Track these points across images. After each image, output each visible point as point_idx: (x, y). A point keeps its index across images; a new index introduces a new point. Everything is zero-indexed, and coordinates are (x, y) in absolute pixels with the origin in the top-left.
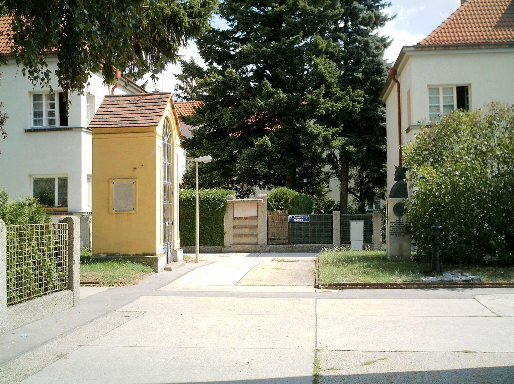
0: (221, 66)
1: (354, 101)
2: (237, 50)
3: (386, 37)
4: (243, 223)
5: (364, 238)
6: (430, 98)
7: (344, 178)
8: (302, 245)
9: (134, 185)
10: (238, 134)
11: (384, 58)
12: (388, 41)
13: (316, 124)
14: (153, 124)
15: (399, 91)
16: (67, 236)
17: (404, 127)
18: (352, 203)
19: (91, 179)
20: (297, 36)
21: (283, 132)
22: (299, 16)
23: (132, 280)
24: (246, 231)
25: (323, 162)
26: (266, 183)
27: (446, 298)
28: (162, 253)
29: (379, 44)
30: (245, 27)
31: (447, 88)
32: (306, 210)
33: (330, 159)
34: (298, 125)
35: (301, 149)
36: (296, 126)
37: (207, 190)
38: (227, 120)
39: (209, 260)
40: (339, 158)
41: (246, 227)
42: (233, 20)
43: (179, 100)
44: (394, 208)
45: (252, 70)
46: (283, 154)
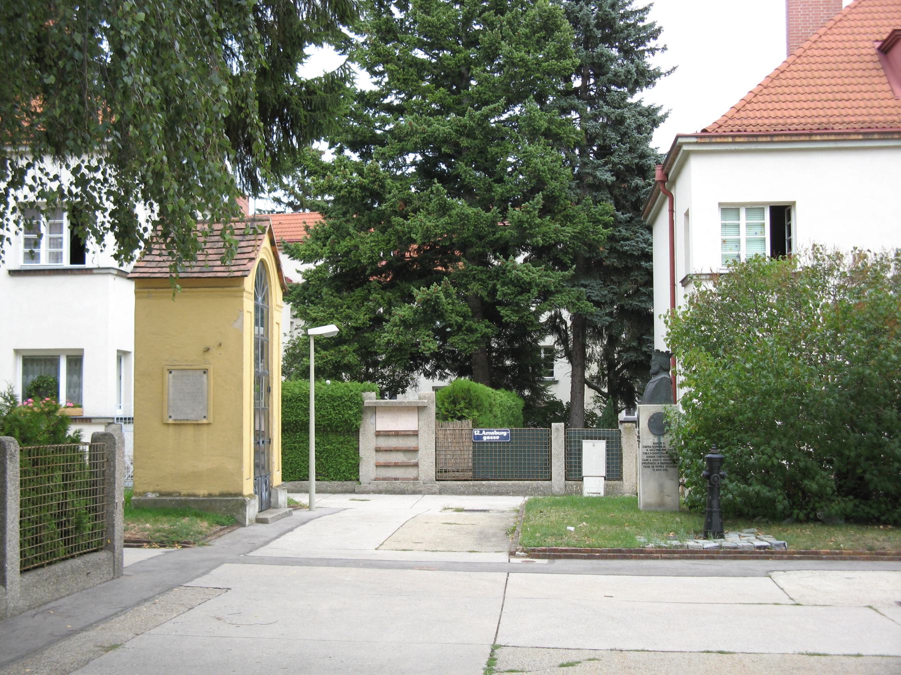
0: (358, 154)
1: (596, 222)
2: (387, 128)
3: (656, 106)
4: (393, 442)
5: (608, 471)
6: (724, 226)
7: (578, 360)
8: (511, 482)
9: (205, 376)
10: (386, 278)
11: (652, 145)
12: (660, 114)
13: (528, 264)
14: (239, 274)
15: (672, 211)
16: (105, 464)
17: (679, 276)
18: (593, 406)
19: (130, 363)
20: (494, 105)
21: (467, 276)
22: (500, 68)
23: (200, 539)
24: (399, 458)
25: (543, 331)
26: (437, 367)
27: (722, 576)
28: (252, 492)
29: (643, 120)
30: (403, 86)
31: (753, 208)
32: (505, 418)
33: (554, 325)
34: (496, 263)
35: (499, 308)
36: (492, 265)
37: (328, 382)
38: (365, 254)
39: (333, 506)
40: (569, 323)
41: (397, 450)
42: (381, 73)
43: (280, 208)
44: (649, 421)
45: (414, 163)
46: (465, 317)
